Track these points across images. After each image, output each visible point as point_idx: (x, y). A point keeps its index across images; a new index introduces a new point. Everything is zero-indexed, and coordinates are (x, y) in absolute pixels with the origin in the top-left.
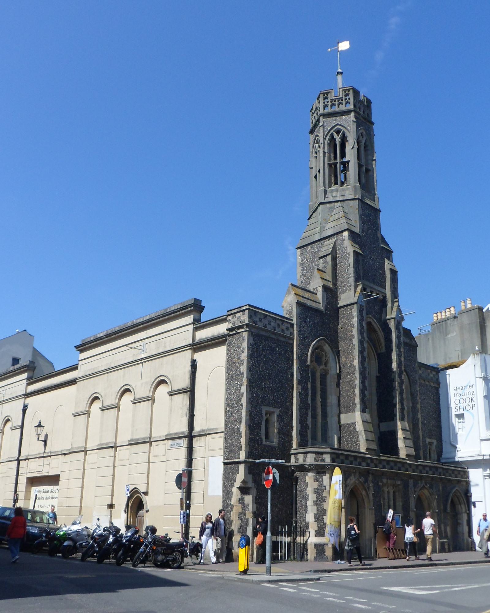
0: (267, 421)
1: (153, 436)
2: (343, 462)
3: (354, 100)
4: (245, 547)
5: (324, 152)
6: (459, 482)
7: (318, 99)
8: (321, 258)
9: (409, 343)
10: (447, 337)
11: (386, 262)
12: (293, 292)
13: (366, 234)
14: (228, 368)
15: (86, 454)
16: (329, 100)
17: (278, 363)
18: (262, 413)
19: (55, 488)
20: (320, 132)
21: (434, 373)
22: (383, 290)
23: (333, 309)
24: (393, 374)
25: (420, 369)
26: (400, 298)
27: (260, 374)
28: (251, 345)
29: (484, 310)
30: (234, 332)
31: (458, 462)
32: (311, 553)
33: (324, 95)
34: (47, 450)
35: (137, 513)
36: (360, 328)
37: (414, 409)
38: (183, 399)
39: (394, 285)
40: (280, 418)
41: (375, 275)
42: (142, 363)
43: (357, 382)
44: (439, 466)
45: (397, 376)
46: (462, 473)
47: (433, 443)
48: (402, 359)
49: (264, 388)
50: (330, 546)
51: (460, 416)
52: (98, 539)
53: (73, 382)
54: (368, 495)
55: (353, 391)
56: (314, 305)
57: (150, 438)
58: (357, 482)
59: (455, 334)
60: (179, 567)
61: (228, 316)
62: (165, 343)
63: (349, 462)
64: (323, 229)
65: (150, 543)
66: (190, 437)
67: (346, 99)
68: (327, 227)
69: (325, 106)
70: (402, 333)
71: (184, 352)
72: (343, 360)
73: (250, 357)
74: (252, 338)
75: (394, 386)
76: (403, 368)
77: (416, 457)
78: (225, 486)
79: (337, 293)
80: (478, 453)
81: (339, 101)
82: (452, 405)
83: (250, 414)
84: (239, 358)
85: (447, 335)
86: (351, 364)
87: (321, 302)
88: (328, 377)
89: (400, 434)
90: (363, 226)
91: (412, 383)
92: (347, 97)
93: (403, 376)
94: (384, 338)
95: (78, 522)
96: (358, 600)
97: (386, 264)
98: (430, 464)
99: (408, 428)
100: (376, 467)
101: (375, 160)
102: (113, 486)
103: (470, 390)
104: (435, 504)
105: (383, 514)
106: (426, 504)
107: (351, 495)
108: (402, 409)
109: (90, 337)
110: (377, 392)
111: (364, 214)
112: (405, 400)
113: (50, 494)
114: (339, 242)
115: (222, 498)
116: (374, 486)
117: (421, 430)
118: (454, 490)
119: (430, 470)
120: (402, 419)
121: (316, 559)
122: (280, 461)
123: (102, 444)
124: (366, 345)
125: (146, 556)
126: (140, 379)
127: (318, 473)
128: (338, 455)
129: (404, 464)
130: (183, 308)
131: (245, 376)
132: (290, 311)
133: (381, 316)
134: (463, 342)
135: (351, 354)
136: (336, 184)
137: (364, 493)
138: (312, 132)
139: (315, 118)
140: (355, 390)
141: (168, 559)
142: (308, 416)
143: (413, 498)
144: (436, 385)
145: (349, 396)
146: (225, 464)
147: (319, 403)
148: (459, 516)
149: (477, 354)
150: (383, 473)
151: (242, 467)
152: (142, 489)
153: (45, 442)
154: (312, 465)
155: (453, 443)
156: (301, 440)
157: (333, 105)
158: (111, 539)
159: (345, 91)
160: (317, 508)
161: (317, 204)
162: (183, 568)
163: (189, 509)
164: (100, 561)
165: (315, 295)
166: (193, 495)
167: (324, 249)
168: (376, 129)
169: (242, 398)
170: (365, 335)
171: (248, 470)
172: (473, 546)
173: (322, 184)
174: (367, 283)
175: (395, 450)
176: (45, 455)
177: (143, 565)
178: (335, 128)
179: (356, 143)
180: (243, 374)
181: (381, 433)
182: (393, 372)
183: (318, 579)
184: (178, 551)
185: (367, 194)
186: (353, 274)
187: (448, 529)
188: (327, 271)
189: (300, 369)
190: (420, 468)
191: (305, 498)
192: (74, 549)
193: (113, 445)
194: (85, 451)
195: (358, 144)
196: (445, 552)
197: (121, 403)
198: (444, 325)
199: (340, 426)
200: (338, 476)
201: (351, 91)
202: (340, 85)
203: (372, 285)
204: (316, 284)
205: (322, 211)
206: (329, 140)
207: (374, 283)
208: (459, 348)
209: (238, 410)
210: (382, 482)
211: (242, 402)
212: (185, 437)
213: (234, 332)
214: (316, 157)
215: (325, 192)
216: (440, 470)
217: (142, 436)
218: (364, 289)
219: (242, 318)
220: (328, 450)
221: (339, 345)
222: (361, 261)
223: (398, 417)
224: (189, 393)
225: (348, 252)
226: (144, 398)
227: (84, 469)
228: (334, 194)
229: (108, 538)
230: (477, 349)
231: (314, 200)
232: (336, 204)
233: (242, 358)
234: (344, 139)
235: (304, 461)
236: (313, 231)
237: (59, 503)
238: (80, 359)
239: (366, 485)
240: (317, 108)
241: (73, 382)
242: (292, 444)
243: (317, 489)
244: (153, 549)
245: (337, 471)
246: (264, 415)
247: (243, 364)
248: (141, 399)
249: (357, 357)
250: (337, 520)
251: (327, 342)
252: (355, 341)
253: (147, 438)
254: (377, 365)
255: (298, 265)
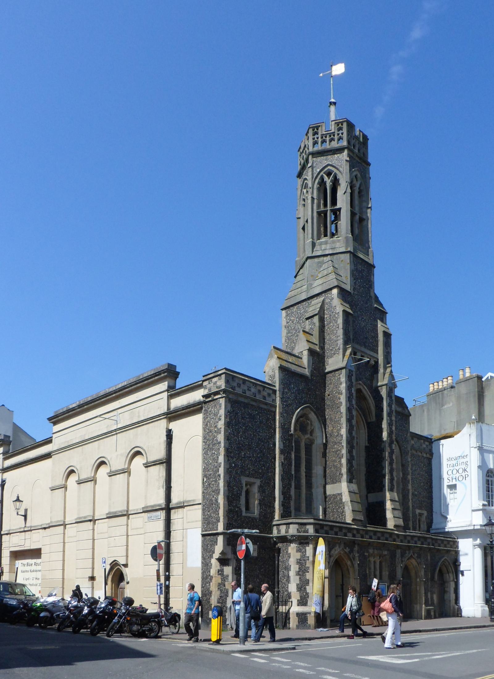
0: (247, 492)
1: (130, 508)
2: (327, 533)
3: (348, 135)
4: (217, 617)
5: (313, 198)
6: (448, 551)
7: (307, 135)
8: (307, 319)
9: (401, 412)
10: (444, 407)
11: (380, 324)
12: (276, 356)
13: (358, 292)
14: (204, 438)
15: (65, 528)
16: (319, 136)
17: (259, 431)
18: (241, 484)
19: (38, 561)
20: (308, 175)
21: (427, 443)
22: (375, 355)
23: (319, 375)
24: (383, 444)
25: (412, 439)
26: (393, 363)
27: (239, 443)
28: (228, 412)
29: (483, 379)
30: (210, 399)
31: (448, 532)
32: (293, 622)
33: (313, 130)
34: (28, 525)
35: (119, 585)
36: (348, 395)
37: (404, 480)
38: (160, 470)
39: (387, 349)
40: (262, 490)
41: (366, 338)
42: (117, 434)
43: (344, 451)
44: (428, 536)
45: (387, 445)
46: (451, 543)
47: (423, 514)
48: (394, 428)
49: (244, 458)
50: (313, 614)
51: (453, 487)
52: (74, 610)
53: (48, 456)
54: (353, 565)
55: (340, 461)
56: (299, 370)
57: (127, 511)
58: (342, 553)
59: (451, 405)
60: (157, 637)
61: (203, 381)
62: (139, 413)
63: (333, 532)
64: (310, 287)
65: (124, 614)
66: (168, 509)
67: (338, 134)
68: (315, 285)
69: (315, 143)
70: (394, 401)
71: (159, 422)
72: (329, 429)
73: (228, 425)
74: (229, 405)
75: (383, 456)
76: (394, 438)
77: (405, 528)
78: (203, 558)
79: (324, 357)
80: (469, 523)
81: (330, 136)
82: (445, 476)
83: (229, 485)
84: (216, 426)
85: (443, 406)
86: (338, 433)
87: (306, 367)
88: (314, 447)
89: (389, 505)
90: (355, 283)
91: (403, 453)
92: (341, 132)
93: (394, 446)
94: (372, 403)
95: (54, 594)
96: (330, 671)
97: (379, 326)
98: (419, 535)
99: (397, 499)
100: (362, 537)
101: (370, 208)
102: (93, 559)
103: (464, 460)
104: (423, 573)
105: (369, 584)
106: (413, 574)
107: (335, 566)
108: (391, 480)
109: (63, 409)
110: (366, 463)
111: (357, 270)
112: (395, 471)
113: (34, 568)
114: (327, 301)
115: (201, 570)
116: (359, 557)
117: (411, 501)
118: (443, 560)
119: (419, 540)
120: (391, 490)
121: (298, 627)
122: (254, 531)
123: (80, 518)
124: (354, 413)
125: (121, 626)
126: (115, 451)
127: (300, 543)
128: (322, 526)
129: (391, 534)
130: (155, 375)
131: (222, 445)
132: (273, 377)
133: (372, 382)
134: (459, 413)
135: (338, 422)
136: (326, 235)
137: (349, 563)
138: (300, 175)
139: (303, 159)
140: (342, 460)
141: (144, 629)
142: (291, 487)
143: (400, 567)
144: (428, 456)
145: (335, 467)
146: (203, 535)
147: (303, 474)
148: (446, 585)
149: (473, 423)
150: (369, 543)
151: (220, 539)
152: (122, 561)
153: (25, 516)
154: (294, 536)
155: (443, 514)
156: (284, 511)
157: (323, 142)
158: (86, 610)
159: (337, 124)
160: (300, 578)
161: (304, 259)
162: (160, 637)
163: (169, 581)
164: (75, 632)
165: (300, 360)
166: (172, 567)
167: (311, 309)
168: (373, 171)
169: (220, 469)
170: (354, 402)
171: (228, 541)
172: (459, 612)
173: (310, 236)
174: (358, 347)
175: (383, 521)
176: (25, 529)
177: (119, 635)
178: (326, 169)
179: (349, 187)
180: (220, 443)
181: (369, 504)
182: (384, 441)
183: (294, 649)
184: (154, 621)
185: (360, 247)
186: (342, 336)
187: (435, 597)
188: (314, 333)
189: (282, 438)
190: (409, 538)
191: (288, 568)
192: (50, 620)
193: (91, 518)
194: (64, 525)
195: (351, 188)
196: (431, 618)
197: (98, 475)
198: (440, 395)
199: (326, 497)
200: (321, 547)
201: (345, 125)
202: (333, 117)
203: (363, 349)
204: (302, 348)
205: (310, 266)
206: (319, 183)
207: (365, 347)
208: (454, 419)
209: (216, 481)
210: (368, 552)
211: (220, 472)
212: (162, 509)
213: (210, 399)
214: (304, 205)
215: (314, 245)
216: (429, 540)
217: (120, 509)
218: (354, 353)
219: (219, 384)
220: (312, 521)
221: (326, 413)
222: (351, 322)
223: (387, 487)
224: (165, 464)
225: (337, 312)
226: (120, 470)
227: (64, 543)
228: (323, 247)
229: (82, 609)
230: (473, 417)
231: (302, 256)
232: (325, 258)
233: (219, 427)
234: (336, 183)
235: (287, 532)
236: (299, 289)
237: (42, 575)
238: (54, 431)
239: (351, 556)
240: (305, 146)
241: (48, 456)
242: (274, 515)
243: (300, 560)
244: (127, 620)
245: (321, 540)
246: (244, 485)
247: (220, 433)
248: (117, 471)
249: (344, 425)
250: (321, 589)
251: (312, 410)
252: (343, 409)
253: (124, 511)
254: (367, 434)
255: (283, 328)
